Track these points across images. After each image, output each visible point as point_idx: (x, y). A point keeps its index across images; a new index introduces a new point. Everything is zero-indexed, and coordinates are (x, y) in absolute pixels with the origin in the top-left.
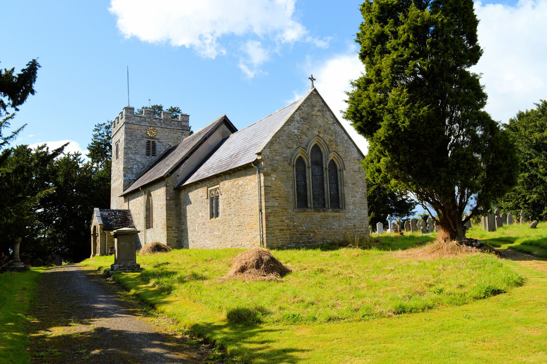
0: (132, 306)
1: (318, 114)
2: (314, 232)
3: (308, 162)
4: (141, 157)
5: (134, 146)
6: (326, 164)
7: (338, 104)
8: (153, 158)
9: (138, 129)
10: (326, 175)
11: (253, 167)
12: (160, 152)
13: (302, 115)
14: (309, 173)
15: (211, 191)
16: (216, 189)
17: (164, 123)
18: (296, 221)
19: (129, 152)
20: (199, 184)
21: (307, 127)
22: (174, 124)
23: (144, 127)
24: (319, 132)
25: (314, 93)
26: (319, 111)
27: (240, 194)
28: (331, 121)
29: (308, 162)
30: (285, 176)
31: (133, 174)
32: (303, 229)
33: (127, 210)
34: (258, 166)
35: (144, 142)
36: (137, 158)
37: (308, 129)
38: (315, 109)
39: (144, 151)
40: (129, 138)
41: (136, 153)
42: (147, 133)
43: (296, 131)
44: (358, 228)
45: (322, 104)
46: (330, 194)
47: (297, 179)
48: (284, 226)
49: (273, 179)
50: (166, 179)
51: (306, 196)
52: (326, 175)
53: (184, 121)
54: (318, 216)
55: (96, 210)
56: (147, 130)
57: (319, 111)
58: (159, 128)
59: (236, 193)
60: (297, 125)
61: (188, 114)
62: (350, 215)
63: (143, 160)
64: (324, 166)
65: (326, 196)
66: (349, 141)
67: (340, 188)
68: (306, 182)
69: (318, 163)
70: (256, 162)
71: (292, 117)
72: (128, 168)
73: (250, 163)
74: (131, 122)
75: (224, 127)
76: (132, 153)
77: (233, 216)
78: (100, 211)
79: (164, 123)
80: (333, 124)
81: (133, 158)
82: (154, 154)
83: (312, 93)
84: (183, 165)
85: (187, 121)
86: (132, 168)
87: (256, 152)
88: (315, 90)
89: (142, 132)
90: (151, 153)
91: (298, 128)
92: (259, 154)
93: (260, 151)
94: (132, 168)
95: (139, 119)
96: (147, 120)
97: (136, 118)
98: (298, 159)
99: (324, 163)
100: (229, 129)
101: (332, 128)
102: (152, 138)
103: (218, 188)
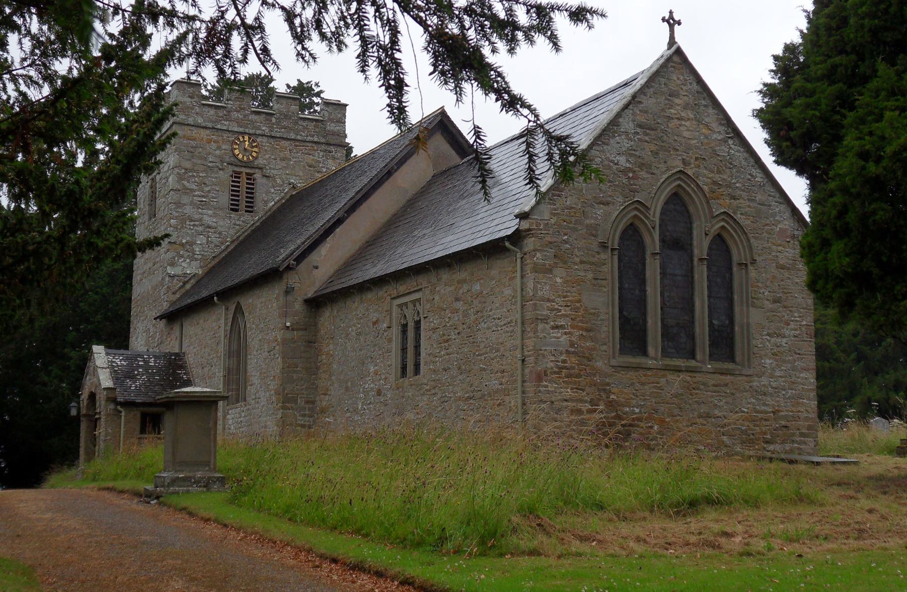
0: (381, 19)
1: (683, 114)
2: (662, 422)
3: (653, 241)
4: (215, 215)
5: (199, 185)
6: (701, 246)
7: (740, 83)
8: (247, 217)
9: (209, 141)
10: (701, 274)
11: (508, 250)
12: (266, 202)
13: (641, 119)
14: (653, 270)
15: (400, 306)
16: (414, 302)
17: (278, 124)
18: (614, 390)
19: (185, 199)
20: (369, 289)
21: (653, 147)
22: (305, 128)
23: (225, 135)
24: (684, 162)
25: (676, 59)
26: (686, 107)
27: (473, 318)
28: (719, 132)
29: (653, 241)
30: (590, 276)
31: (193, 259)
32: (634, 413)
33: (177, 355)
34: (521, 249)
35: (225, 176)
36: (206, 218)
37: (655, 154)
38: (677, 101)
39: (225, 199)
40: (188, 165)
41: (202, 205)
42: (233, 150)
43: (622, 160)
44: (785, 418)
45: (695, 87)
46: (711, 324)
47: (620, 283)
48: (582, 401)
49: (558, 280)
50: (285, 276)
51: (644, 331)
52: (701, 274)
53: (332, 120)
54: (676, 382)
55: (99, 351)
56: (233, 143)
57: (686, 107)
58: (265, 139)
59: (466, 315)
60: (627, 144)
61: (343, 101)
62: (764, 380)
63: (221, 223)
64: (696, 251)
65: (697, 330)
66: (769, 188)
67: (737, 309)
68: (645, 291)
69: (677, 244)
70: (516, 237)
71: (614, 123)
72: (182, 245)
73: (502, 239)
74: (191, 121)
75: (439, 142)
76: (192, 203)
77: (454, 372)
78: (107, 354)
79: (278, 124)
80: (725, 141)
81: (196, 217)
82: (250, 209)
83: (669, 59)
84: (230, 283)
85: (342, 121)
86: (192, 243)
87: (517, 211)
88: (679, 52)
89: (219, 148)
90: (243, 204)
91: (629, 153)
92: (523, 216)
93: (527, 209)
94: (192, 243)
95: (212, 112)
96: (235, 115)
97: (206, 109)
98: (624, 232)
99: (695, 243)
100: (452, 146)
101: (723, 150)
102: (246, 165)
103: (419, 300)
